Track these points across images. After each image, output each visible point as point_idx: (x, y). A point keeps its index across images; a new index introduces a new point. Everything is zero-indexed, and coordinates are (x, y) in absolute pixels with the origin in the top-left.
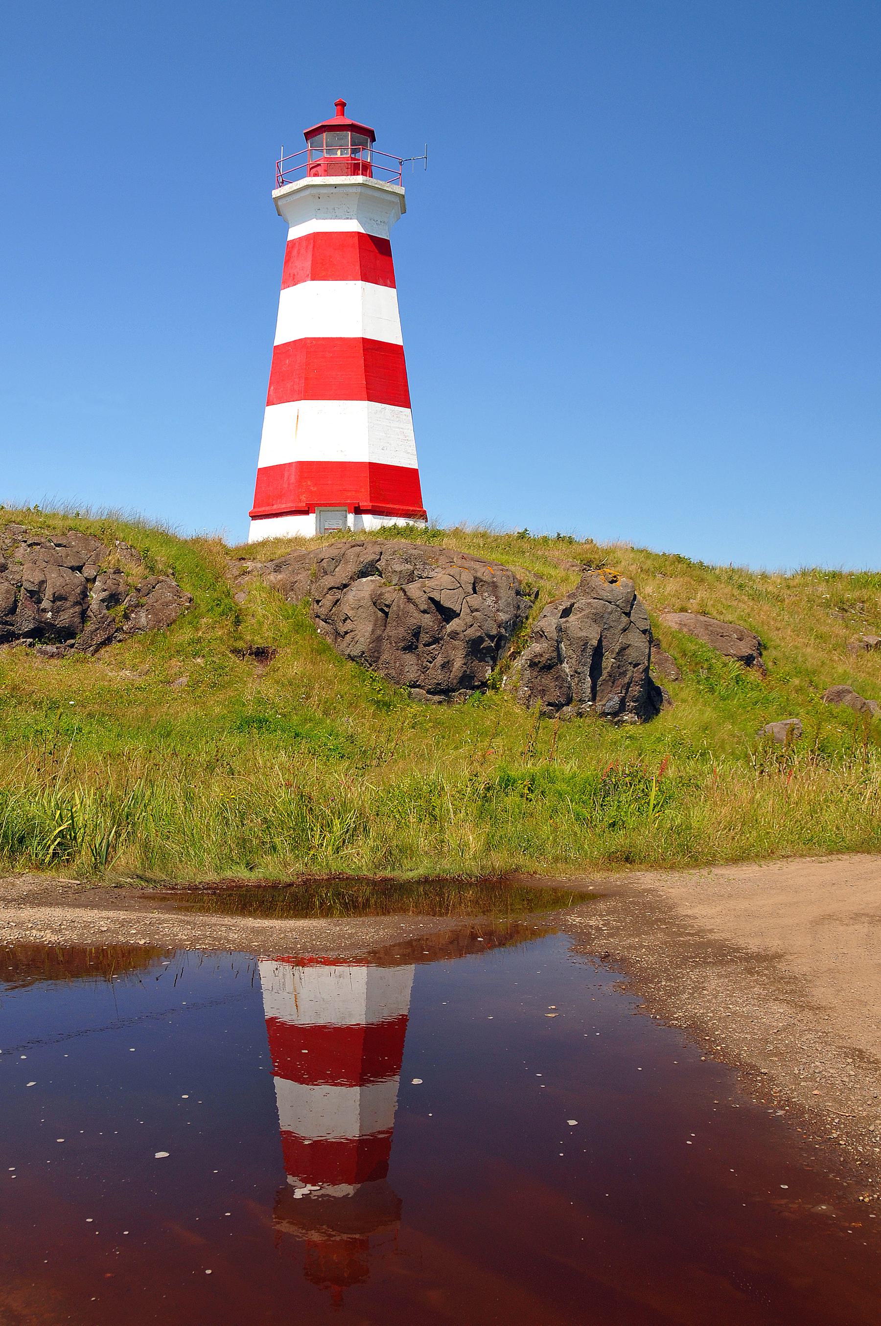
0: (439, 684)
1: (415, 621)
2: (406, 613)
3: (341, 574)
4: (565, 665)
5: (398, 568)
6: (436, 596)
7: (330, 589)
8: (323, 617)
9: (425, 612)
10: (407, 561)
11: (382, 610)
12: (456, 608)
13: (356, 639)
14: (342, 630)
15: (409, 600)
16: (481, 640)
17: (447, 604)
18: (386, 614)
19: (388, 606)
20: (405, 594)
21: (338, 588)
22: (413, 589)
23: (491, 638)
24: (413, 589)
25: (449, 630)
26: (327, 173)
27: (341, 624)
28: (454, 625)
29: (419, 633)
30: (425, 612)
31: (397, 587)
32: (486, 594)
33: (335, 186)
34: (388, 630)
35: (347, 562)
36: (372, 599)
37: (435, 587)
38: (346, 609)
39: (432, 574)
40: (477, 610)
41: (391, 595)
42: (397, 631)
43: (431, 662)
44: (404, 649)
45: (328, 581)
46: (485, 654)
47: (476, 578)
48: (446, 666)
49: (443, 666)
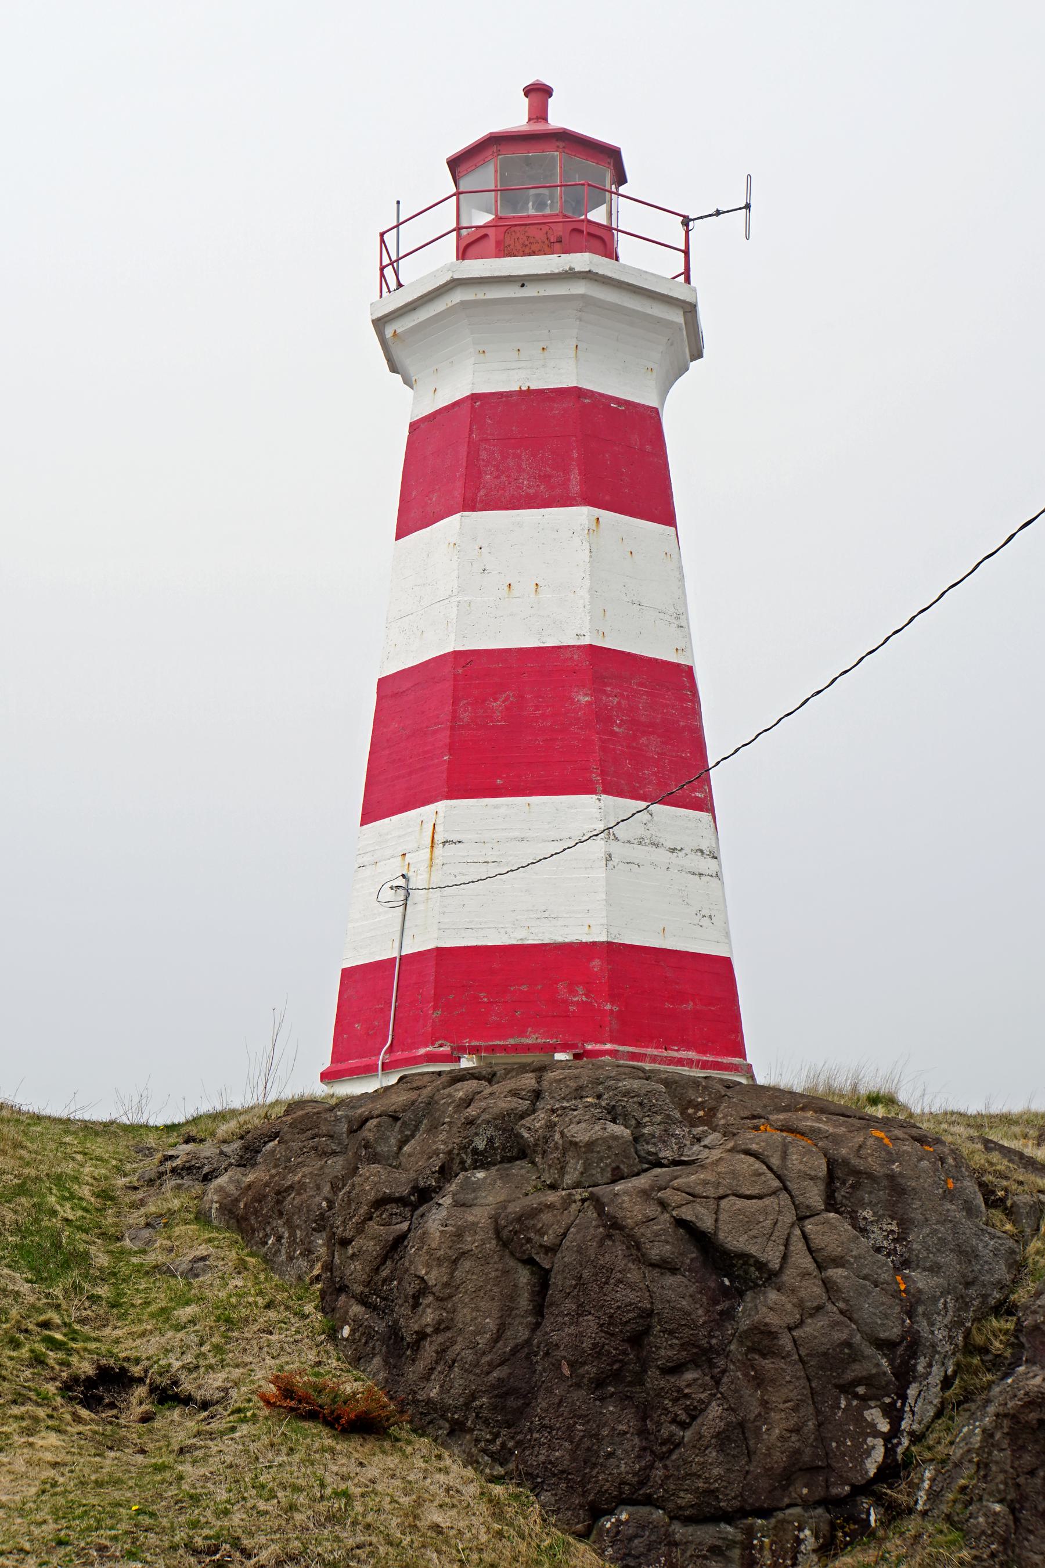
0: (711, 1492)
1: (632, 1296)
2: (606, 1274)
3: (420, 1155)
4: (432, 1395)
5: (581, 1132)
6: (702, 1216)
7: (380, 1203)
8: (358, 1289)
9: (666, 1266)
10: (613, 1114)
11: (530, 1262)
12: (772, 1257)
13: (450, 1355)
14: (410, 1327)
15: (613, 1226)
16: (849, 1353)
17: (735, 1241)
18: (543, 1279)
19: (551, 1250)
20: (601, 1212)
21: (401, 1201)
22: (627, 1196)
23: (885, 1345)
24: (627, 1196)
25: (745, 1324)
26: (503, 251)
27: (406, 1311)
28: (769, 1308)
29: (647, 1331)
30: (666, 1266)
31: (579, 1194)
32: (868, 1214)
33: (523, 281)
34: (547, 1325)
35: (433, 1128)
36: (498, 1232)
37: (699, 1190)
38: (418, 1264)
39: (694, 1151)
40: (838, 1262)
41: (566, 1223)
42: (571, 1331)
43: (684, 1426)
44: (599, 1383)
45: (373, 1179)
46: (863, 1399)
47: (832, 1164)
48: (737, 1436)
49: (722, 1439)
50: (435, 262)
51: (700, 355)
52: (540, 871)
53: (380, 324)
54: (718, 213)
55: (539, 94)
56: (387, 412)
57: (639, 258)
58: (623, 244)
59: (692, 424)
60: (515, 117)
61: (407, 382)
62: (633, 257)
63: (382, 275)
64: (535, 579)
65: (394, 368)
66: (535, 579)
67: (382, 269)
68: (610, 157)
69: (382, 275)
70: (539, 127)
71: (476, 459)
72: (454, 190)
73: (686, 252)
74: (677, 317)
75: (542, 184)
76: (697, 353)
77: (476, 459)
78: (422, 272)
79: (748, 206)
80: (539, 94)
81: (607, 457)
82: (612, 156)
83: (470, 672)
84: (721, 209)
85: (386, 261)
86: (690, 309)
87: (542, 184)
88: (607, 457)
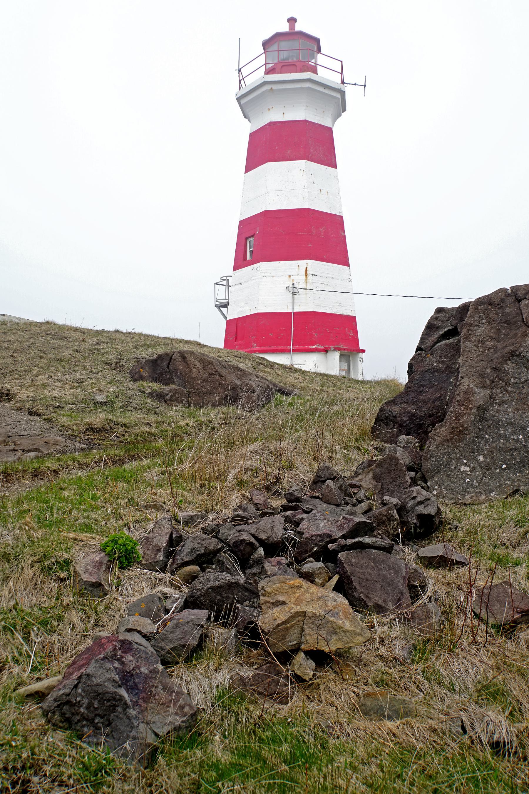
50: (256, 76)
51: (345, 110)
52: (276, 287)
53: (239, 99)
54: (355, 84)
55: (292, 21)
56: (241, 130)
57: (325, 75)
58: (320, 69)
59: (342, 133)
60: (285, 28)
61: (250, 121)
62: (323, 75)
63: (240, 83)
64: (289, 186)
65: (245, 117)
66: (289, 186)
67: (240, 81)
68: (315, 42)
69: (240, 83)
70: (292, 31)
71: (270, 145)
72: (263, 52)
73: (342, 74)
74: (339, 96)
75: (293, 51)
76: (344, 110)
77: (270, 145)
78: (251, 81)
79: (365, 86)
80: (292, 21)
81: (313, 144)
82: (317, 41)
83: (268, 217)
84: (357, 83)
85: (241, 78)
86: (343, 93)
87: (293, 51)
88: (313, 144)
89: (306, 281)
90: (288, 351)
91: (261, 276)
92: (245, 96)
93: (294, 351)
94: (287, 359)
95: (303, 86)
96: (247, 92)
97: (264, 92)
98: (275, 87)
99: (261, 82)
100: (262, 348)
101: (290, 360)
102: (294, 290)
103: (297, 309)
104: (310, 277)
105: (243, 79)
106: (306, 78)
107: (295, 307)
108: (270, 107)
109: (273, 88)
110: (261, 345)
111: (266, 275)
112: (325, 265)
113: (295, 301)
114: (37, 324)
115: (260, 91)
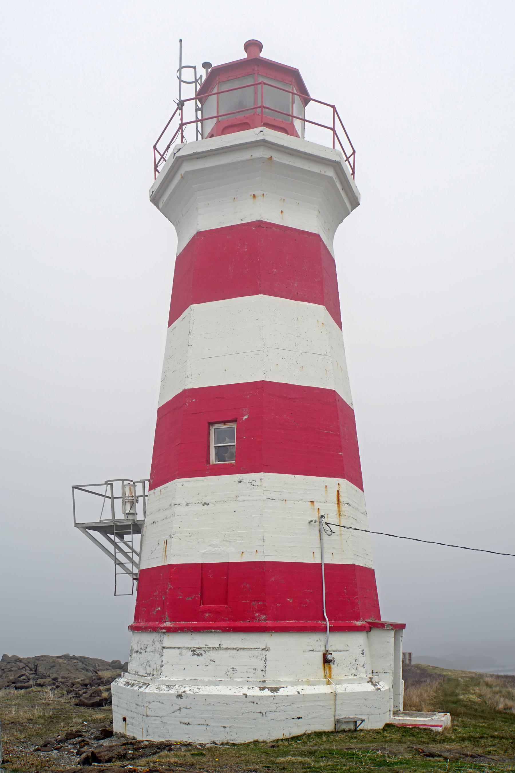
64: (255, 341)
66: (255, 341)
89: (340, 514)
90: (324, 630)
91: (265, 498)
92: (308, 159)
93: (332, 630)
94: (319, 643)
95: (323, 173)
96: (211, 151)
97: (252, 160)
98: (278, 157)
99: (254, 139)
100: (279, 623)
101: (322, 644)
102: (322, 526)
103: (329, 560)
104: (344, 508)
105: (196, 122)
106: (334, 159)
107: (325, 556)
108: (258, 193)
109: (274, 159)
110: (275, 619)
111: (272, 495)
112: (353, 489)
113: (325, 546)
114: (32, 658)
115: (245, 156)
